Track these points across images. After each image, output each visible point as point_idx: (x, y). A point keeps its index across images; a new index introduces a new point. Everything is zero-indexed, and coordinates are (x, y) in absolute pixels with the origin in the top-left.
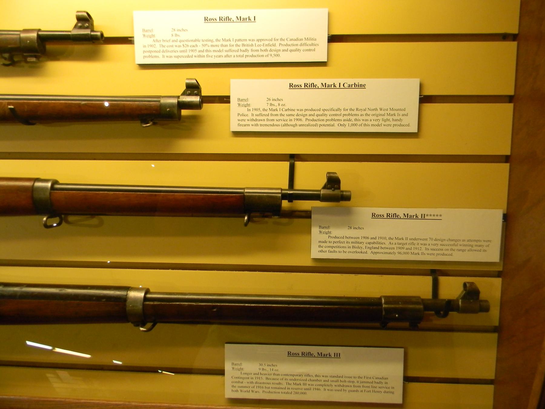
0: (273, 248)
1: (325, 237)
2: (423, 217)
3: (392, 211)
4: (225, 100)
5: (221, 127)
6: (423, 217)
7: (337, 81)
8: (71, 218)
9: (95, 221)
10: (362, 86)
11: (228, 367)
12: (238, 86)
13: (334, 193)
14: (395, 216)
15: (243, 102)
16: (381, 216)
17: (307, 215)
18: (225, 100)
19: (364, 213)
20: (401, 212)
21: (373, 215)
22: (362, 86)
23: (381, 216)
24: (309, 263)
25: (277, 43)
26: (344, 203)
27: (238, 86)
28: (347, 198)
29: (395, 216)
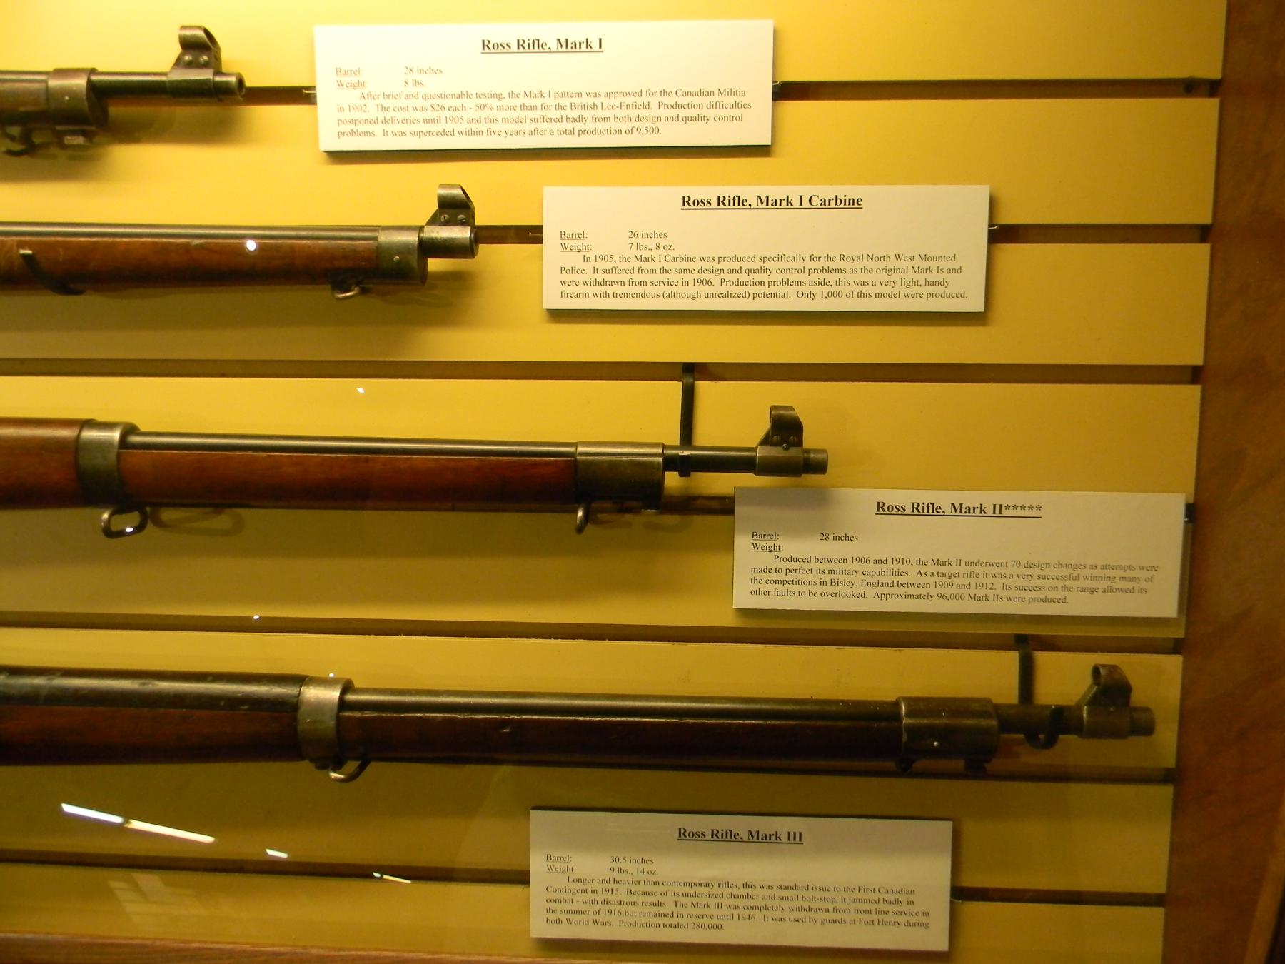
0: (643, 586)
1: (765, 559)
2: (998, 511)
3: (924, 497)
4: (531, 235)
5: (521, 300)
6: (998, 511)
7: (794, 192)
8: (168, 515)
9: (223, 520)
10: (854, 203)
11: (537, 865)
12: (561, 202)
13: (789, 454)
14: (932, 509)
15: (574, 241)
16: (898, 510)
17: (724, 506)
18: (531, 235)
19: (858, 501)
20: (944, 499)
21: (880, 506)
22: (854, 203)
23: (898, 510)
24: (729, 621)
25: (654, 101)
26: (810, 479)
27: (561, 202)
28: (819, 467)
29: (932, 509)
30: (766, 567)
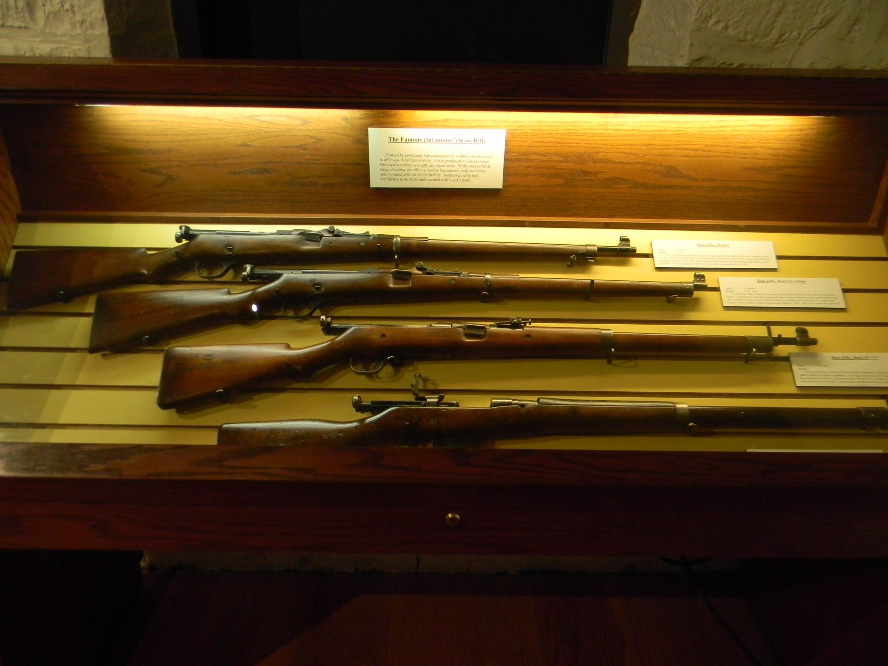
0: (767, 382)
1: (803, 372)
2: (867, 358)
3: (845, 354)
4: (717, 289)
5: (711, 307)
6: (867, 358)
7: (787, 279)
8: (614, 362)
9: (633, 363)
10: (803, 282)
11: (840, 294)
12: (725, 281)
13: (804, 340)
14: (847, 358)
15: (729, 290)
16: (838, 358)
17: (787, 359)
18: (717, 289)
19: (827, 355)
20: (851, 355)
21: (833, 357)
22: (803, 282)
23: (838, 358)
24: (794, 391)
25: (456, 164)
26: (812, 348)
27: (725, 281)
28: (814, 342)
29: (847, 358)
30: (806, 375)
